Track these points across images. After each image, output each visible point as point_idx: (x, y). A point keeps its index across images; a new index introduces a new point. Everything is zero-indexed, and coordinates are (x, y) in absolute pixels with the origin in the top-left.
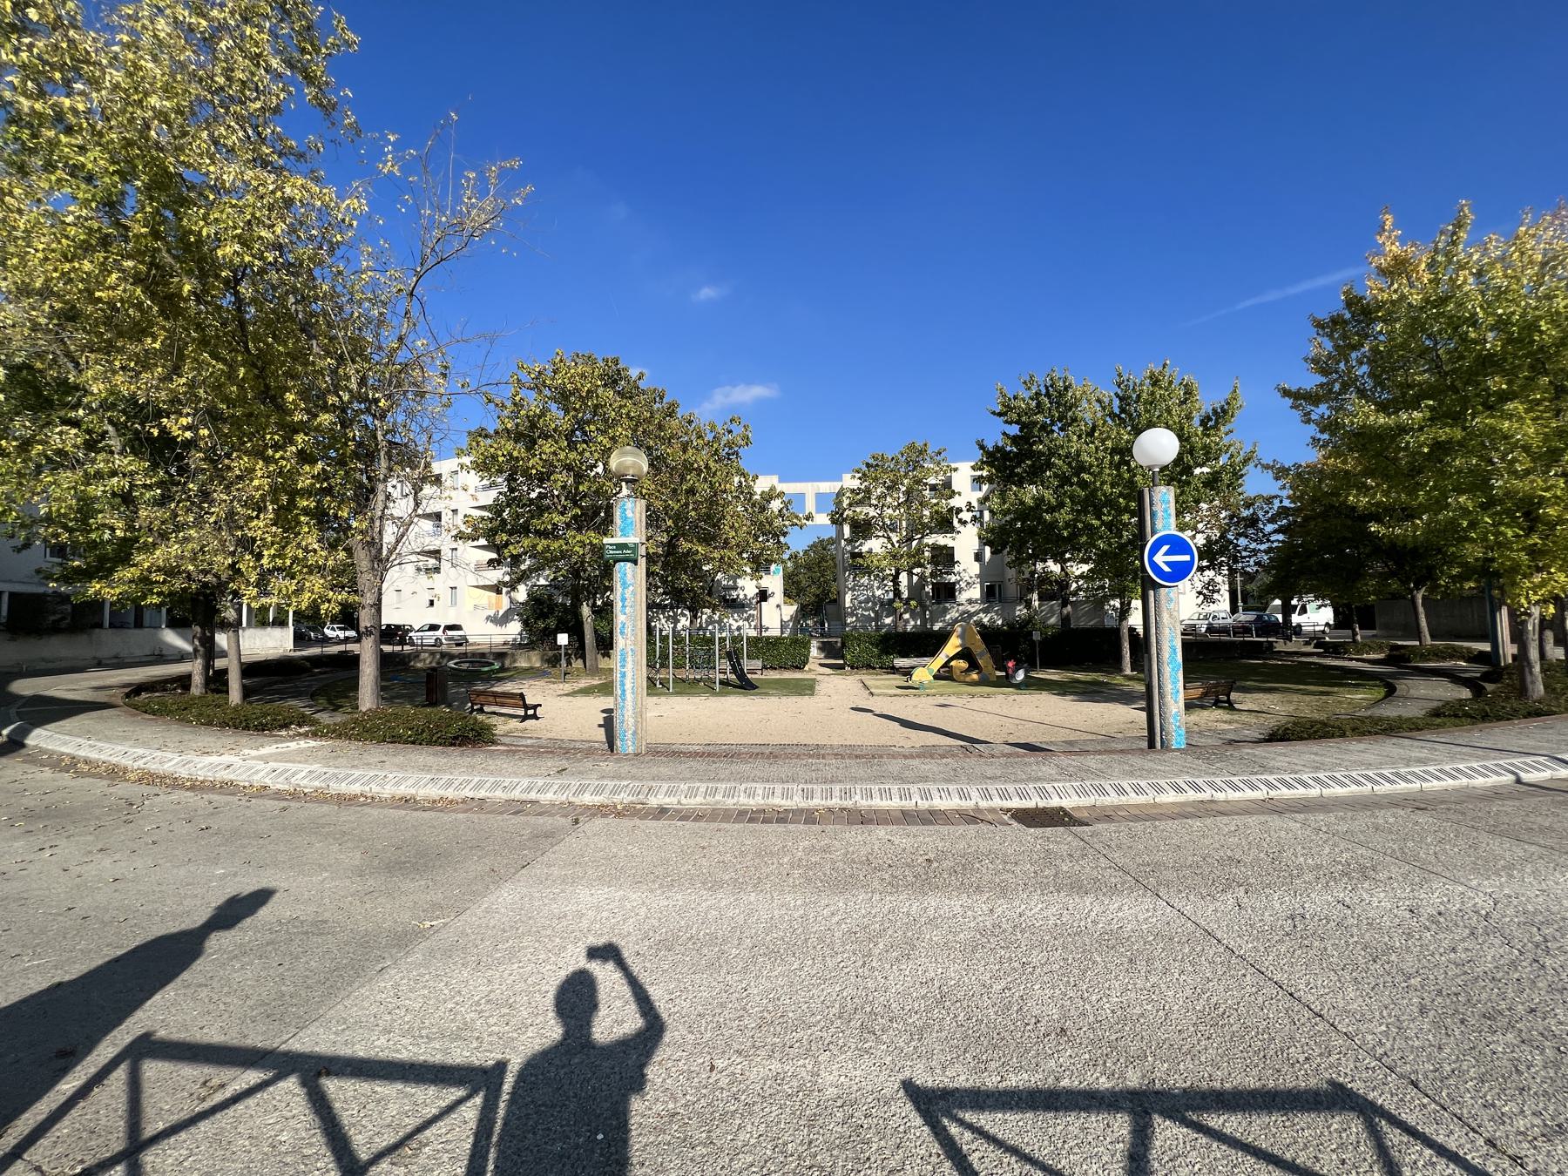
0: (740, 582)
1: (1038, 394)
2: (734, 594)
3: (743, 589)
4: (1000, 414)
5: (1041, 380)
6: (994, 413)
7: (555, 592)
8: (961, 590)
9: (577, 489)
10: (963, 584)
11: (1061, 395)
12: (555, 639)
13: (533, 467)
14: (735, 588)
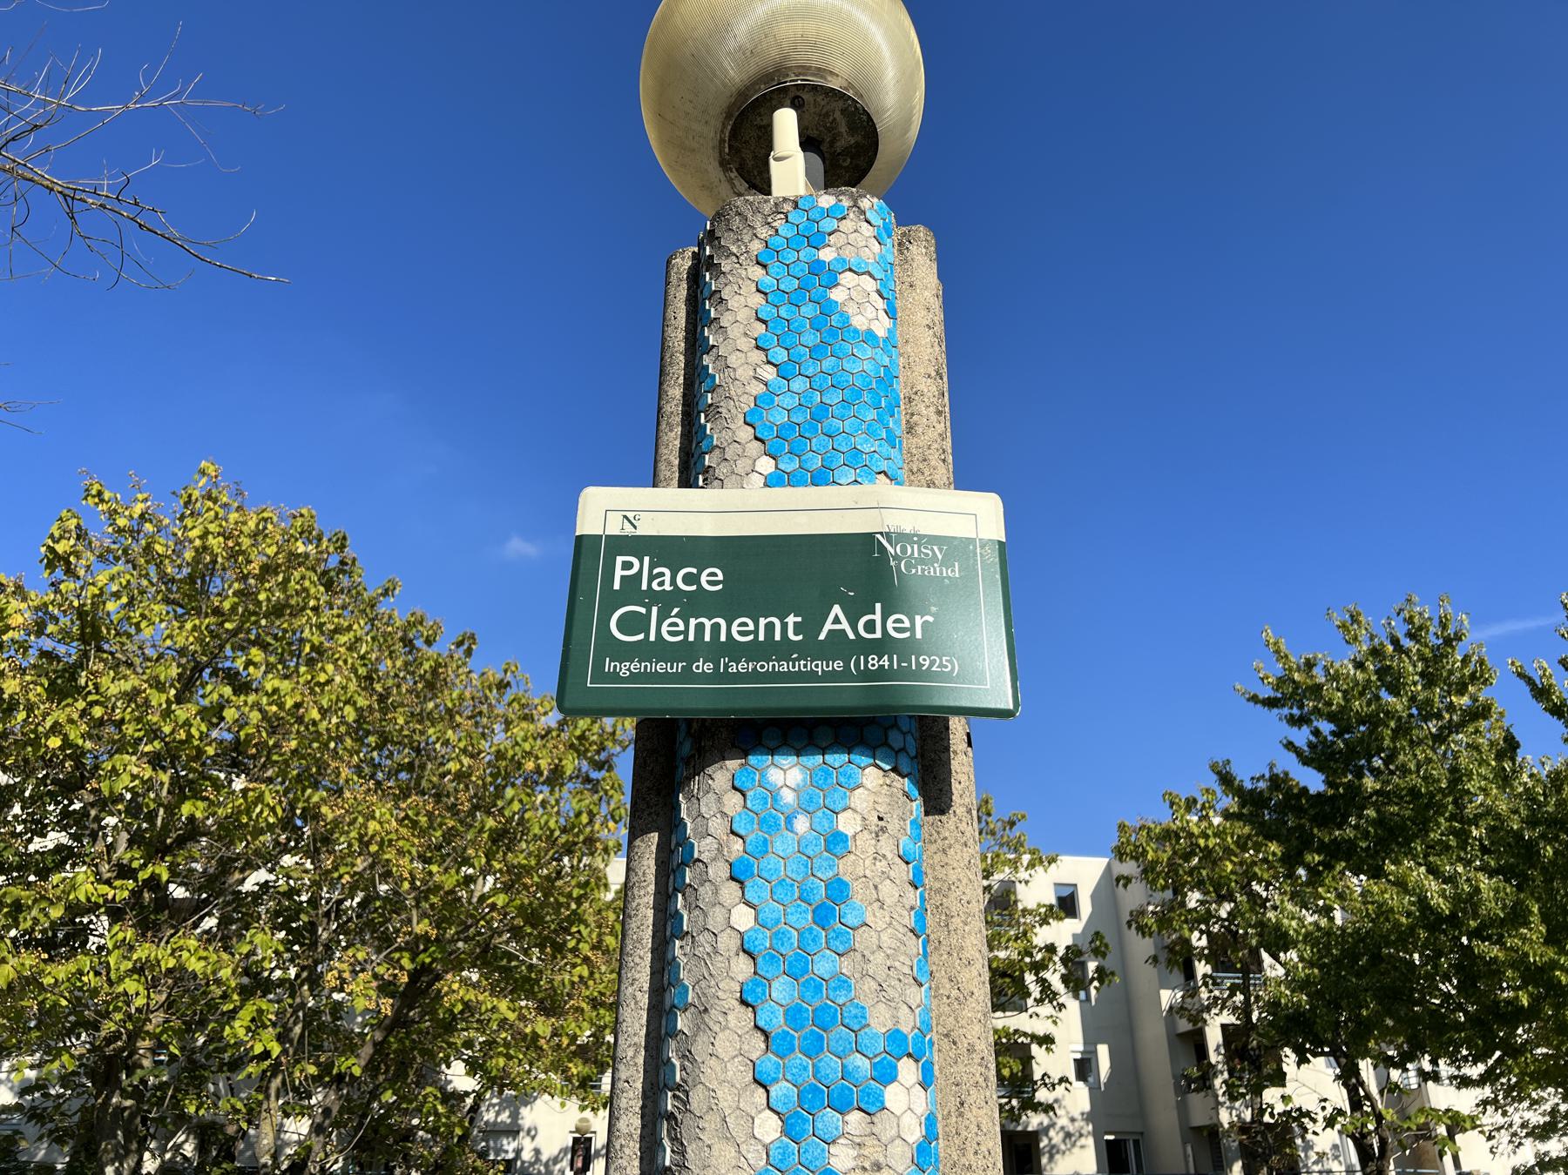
0: (528, 1116)
1: (1376, 652)
2: (509, 1146)
3: (532, 1133)
4: (1271, 703)
5: (1380, 624)
6: (1254, 699)
7: (31, 1129)
8: (1053, 1151)
9: (172, 810)
10: (1056, 1137)
11: (1438, 656)
12: (1102, 1042)
13: (56, 729)
14: (513, 1131)
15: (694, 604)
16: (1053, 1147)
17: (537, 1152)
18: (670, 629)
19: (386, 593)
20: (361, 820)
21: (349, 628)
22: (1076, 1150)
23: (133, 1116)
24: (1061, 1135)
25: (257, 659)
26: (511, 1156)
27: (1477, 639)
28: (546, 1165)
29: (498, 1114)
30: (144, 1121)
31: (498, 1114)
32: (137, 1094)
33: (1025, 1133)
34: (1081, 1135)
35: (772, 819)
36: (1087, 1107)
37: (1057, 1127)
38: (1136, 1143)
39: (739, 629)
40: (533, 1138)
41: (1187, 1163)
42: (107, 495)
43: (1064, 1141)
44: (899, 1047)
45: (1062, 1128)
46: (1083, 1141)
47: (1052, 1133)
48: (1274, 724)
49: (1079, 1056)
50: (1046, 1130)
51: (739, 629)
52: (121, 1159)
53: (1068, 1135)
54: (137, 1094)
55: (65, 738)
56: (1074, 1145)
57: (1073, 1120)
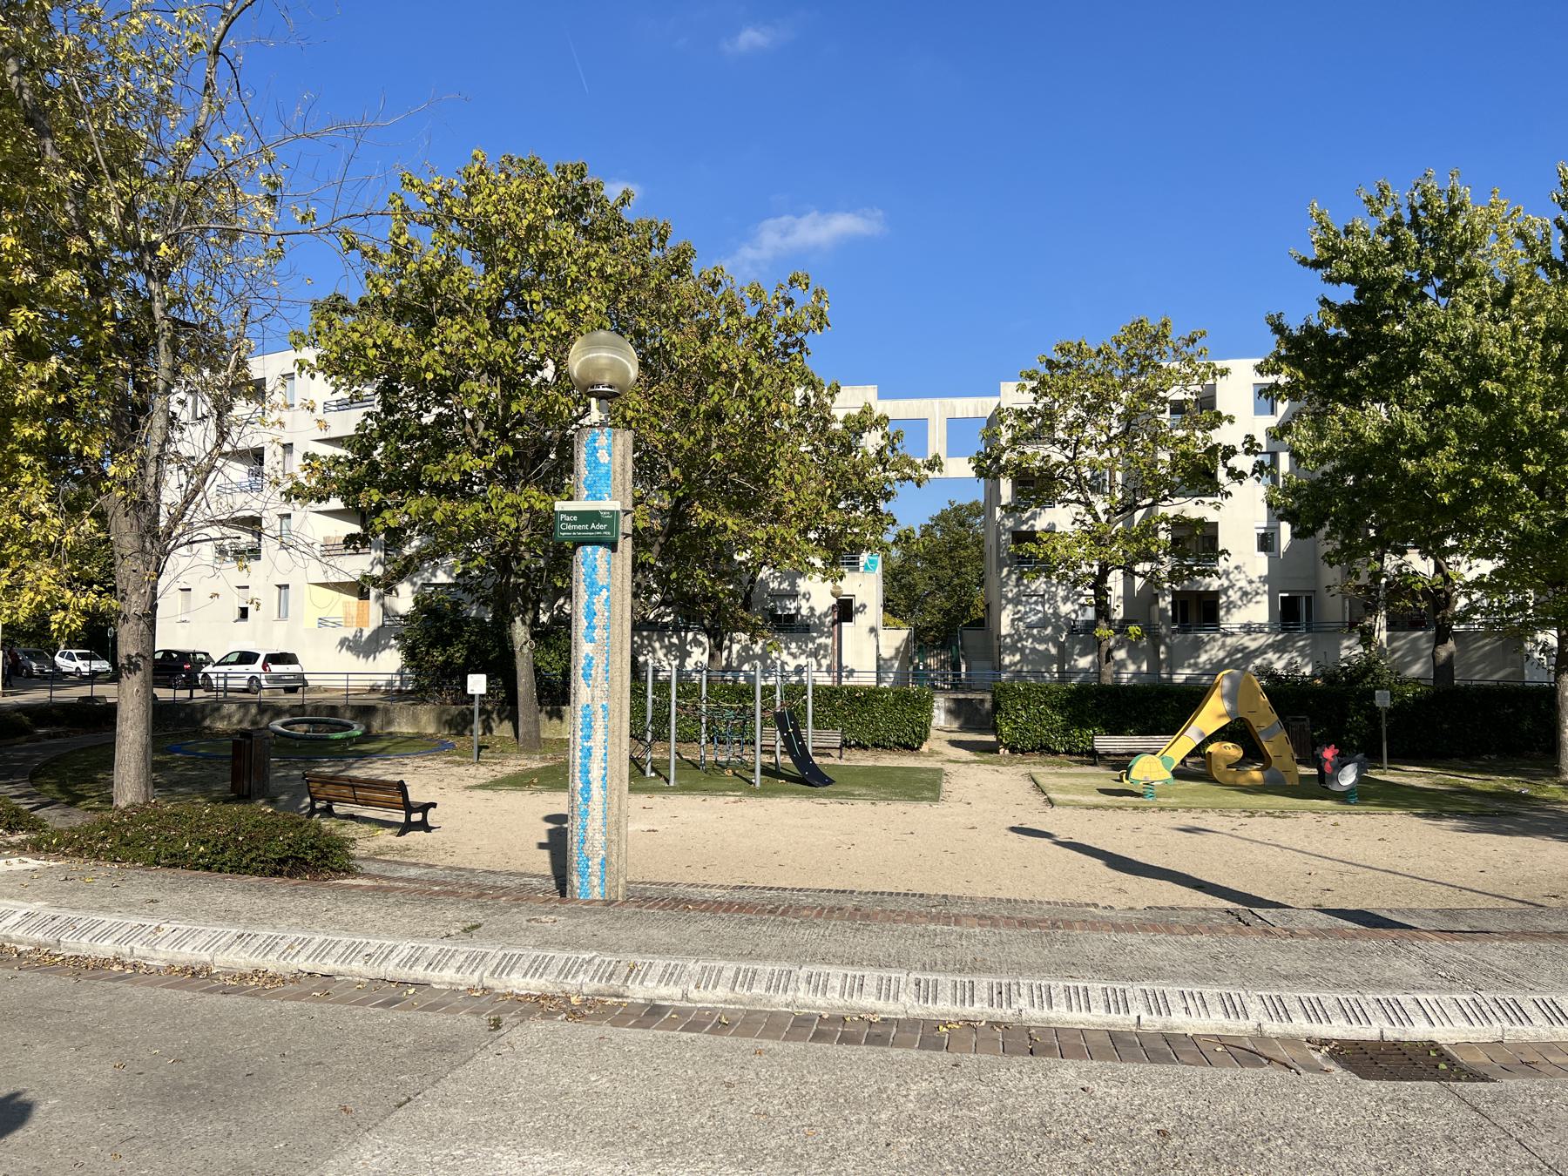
0: (803, 585)
1: (1395, 223)
2: (792, 606)
4: (1316, 264)
5: (1402, 197)
6: (1304, 262)
7: (466, 597)
8: (1230, 606)
10: (1234, 595)
11: (1442, 225)
14: (793, 595)
15: (573, 523)
16: (1232, 602)
17: (812, 609)
18: (569, 527)
19: (623, 202)
20: (621, 409)
21: (597, 253)
22: (1251, 605)
23: (526, 588)
24: (1239, 593)
25: (537, 299)
26: (793, 612)
27: (1475, 213)
28: (819, 618)
29: (780, 583)
30: (534, 591)
31: (780, 583)
32: (524, 575)
33: (1207, 592)
34: (1257, 594)
35: (586, 556)
36: (1265, 572)
37: (1236, 588)
38: (1309, 599)
39: (579, 527)
40: (808, 600)
41: (1344, 613)
42: (415, 182)
43: (1241, 599)
44: (603, 587)
45: (1241, 588)
46: (1258, 598)
47: (1230, 592)
48: (1314, 284)
49: (1263, 531)
50: (1225, 590)
51: (579, 527)
52: (524, 613)
53: (1245, 594)
54: (524, 575)
55: (434, 372)
56: (1250, 601)
57: (1251, 582)
